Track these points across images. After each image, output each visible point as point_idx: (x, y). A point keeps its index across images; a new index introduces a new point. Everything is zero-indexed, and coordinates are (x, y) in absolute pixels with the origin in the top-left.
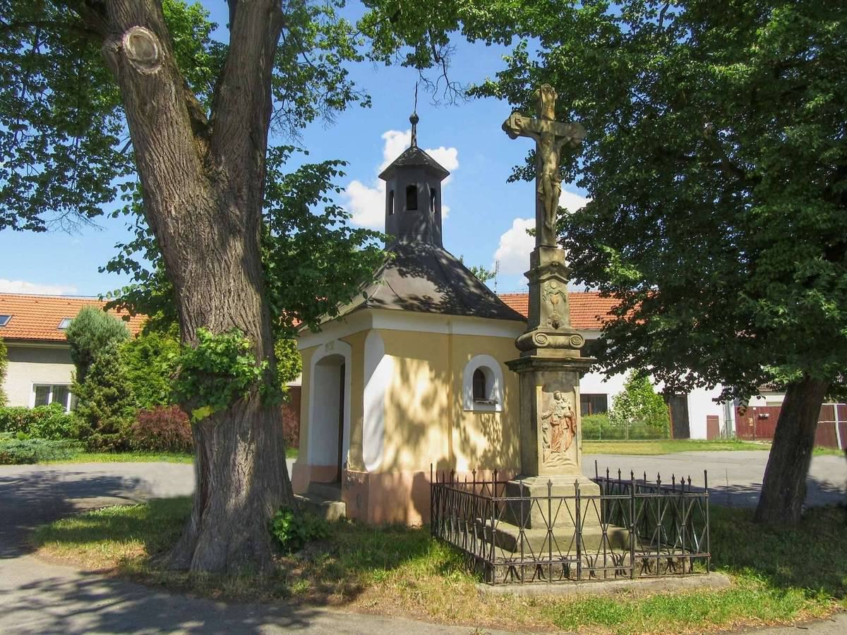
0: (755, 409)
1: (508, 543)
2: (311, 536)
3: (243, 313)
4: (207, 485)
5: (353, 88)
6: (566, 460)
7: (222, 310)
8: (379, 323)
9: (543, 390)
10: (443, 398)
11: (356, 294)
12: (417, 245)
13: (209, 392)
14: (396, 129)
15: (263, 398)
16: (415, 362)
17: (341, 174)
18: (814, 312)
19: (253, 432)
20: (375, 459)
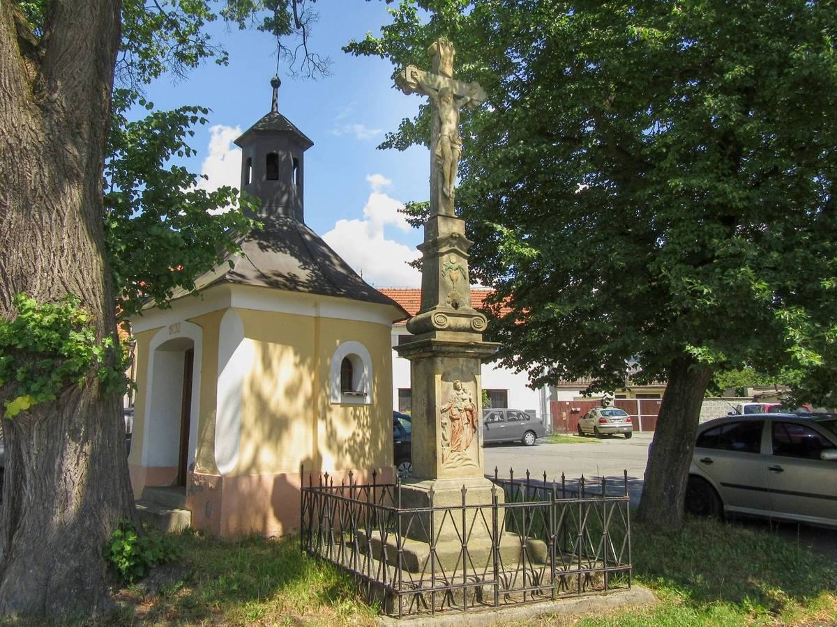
0: (568, 403)
1: (411, 564)
2: (159, 559)
3: (79, 277)
4: (20, 499)
5: (208, 42)
6: (467, 459)
7: (50, 273)
8: (239, 301)
9: (442, 379)
10: (307, 387)
11: (220, 262)
12: (278, 218)
13: (31, 376)
14: (224, 124)
15: (103, 386)
16: (279, 347)
17: (192, 133)
18: (743, 292)
19: (87, 429)
20: (231, 458)
